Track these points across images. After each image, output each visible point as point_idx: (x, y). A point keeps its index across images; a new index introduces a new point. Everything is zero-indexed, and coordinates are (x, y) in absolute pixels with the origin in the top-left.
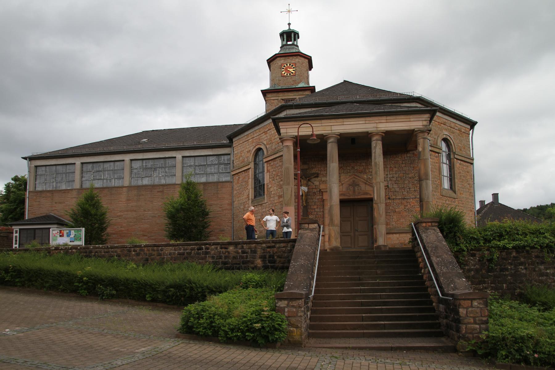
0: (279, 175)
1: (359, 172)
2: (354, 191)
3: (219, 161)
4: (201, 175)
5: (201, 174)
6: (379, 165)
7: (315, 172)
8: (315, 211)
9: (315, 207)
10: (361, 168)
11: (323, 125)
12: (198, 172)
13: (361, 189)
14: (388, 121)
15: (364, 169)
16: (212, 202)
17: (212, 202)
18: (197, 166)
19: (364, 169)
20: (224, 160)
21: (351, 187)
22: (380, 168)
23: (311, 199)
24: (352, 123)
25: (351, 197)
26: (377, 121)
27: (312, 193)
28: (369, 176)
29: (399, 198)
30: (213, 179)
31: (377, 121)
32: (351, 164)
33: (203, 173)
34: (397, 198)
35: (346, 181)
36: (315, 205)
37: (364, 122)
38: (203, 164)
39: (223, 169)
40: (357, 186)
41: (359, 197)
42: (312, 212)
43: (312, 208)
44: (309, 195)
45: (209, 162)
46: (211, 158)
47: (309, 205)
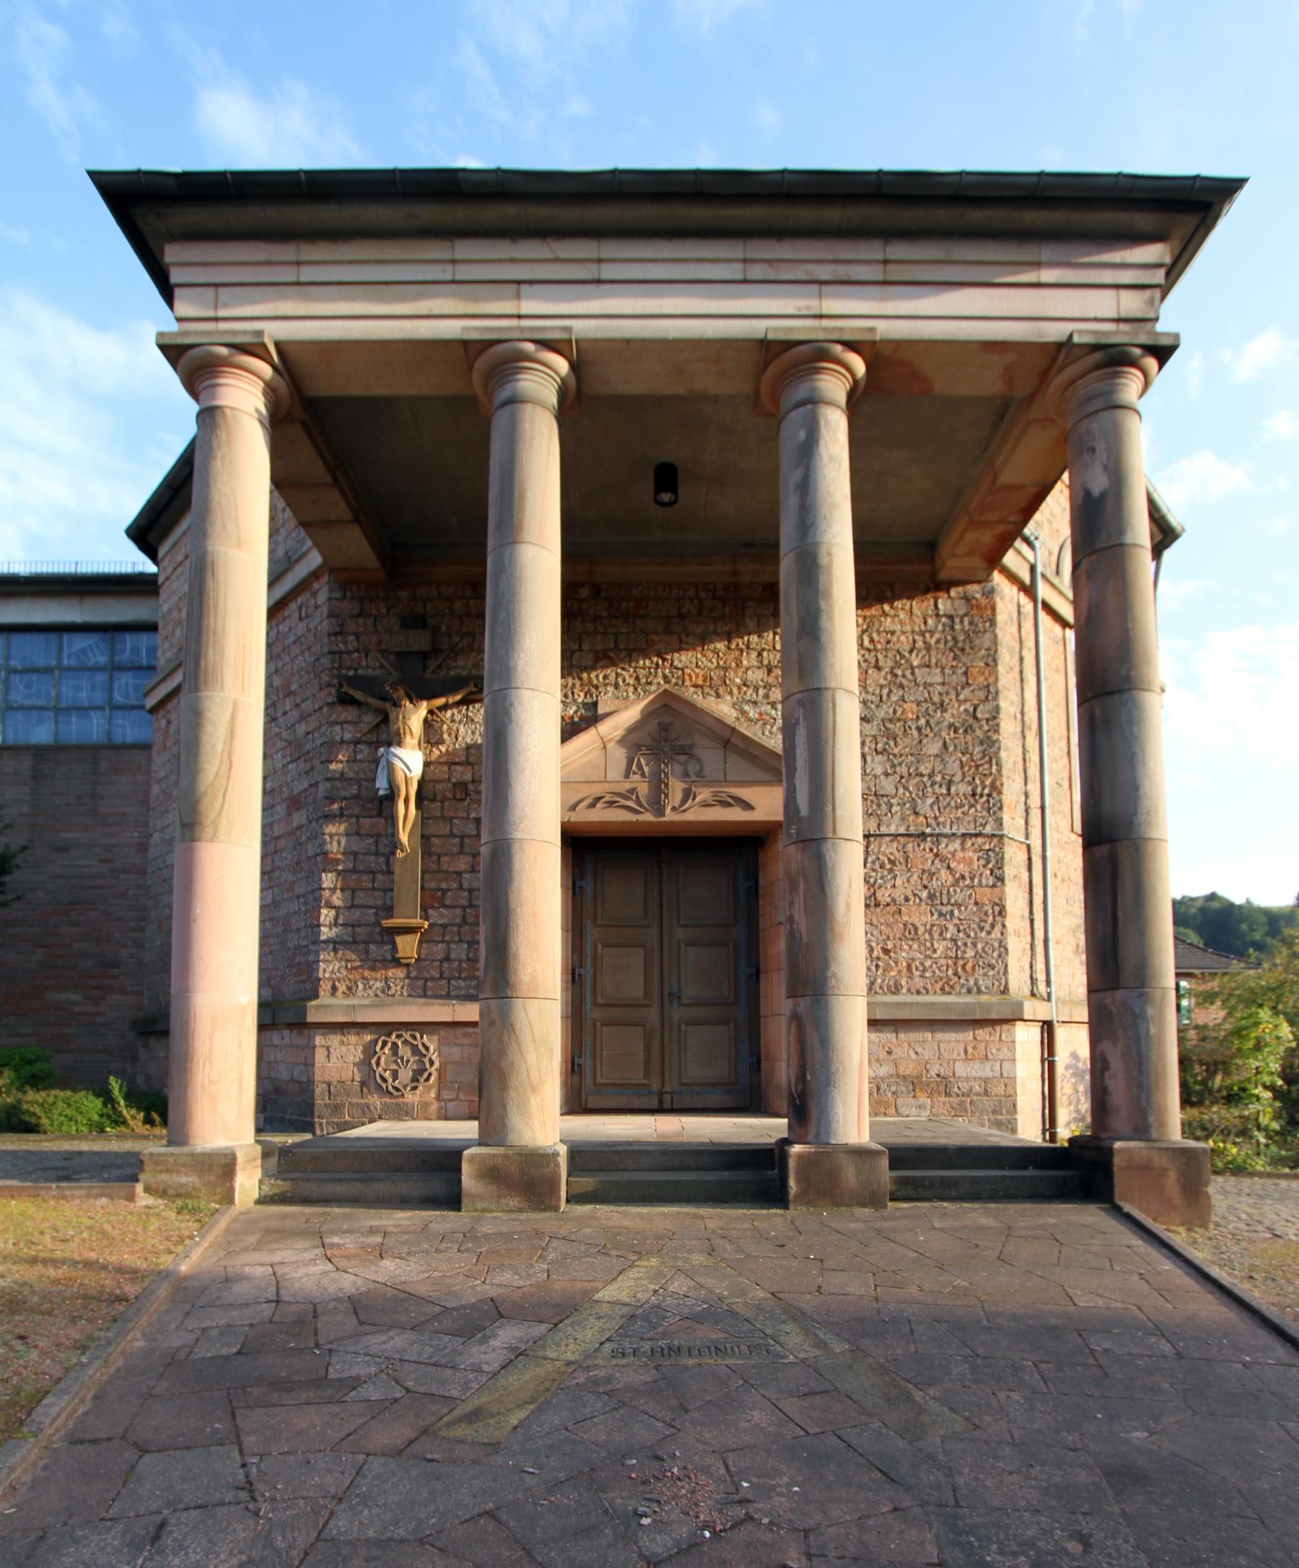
0: (293, 687)
3: (112, 655)
4: (35, 713)
5: (32, 708)
7: (465, 673)
8: (461, 888)
11: (464, 272)
12: (18, 698)
14: (895, 273)
16: (70, 835)
17: (70, 835)
18: (15, 671)
20: (135, 651)
23: (444, 818)
24: (665, 255)
26: (825, 272)
27: (450, 785)
29: (893, 829)
30: (92, 729)
31: (825, 272)
32: (656, 638)
33: (40, 702)
34: (884, 830)
36: (461, 852)
37: (735, 271)
38: (41, 662)
39: (131, 690)
40: (683, 758)
42: (444, 892)
43: (445, 867)
45: (69, 657)
46: (79, 642)
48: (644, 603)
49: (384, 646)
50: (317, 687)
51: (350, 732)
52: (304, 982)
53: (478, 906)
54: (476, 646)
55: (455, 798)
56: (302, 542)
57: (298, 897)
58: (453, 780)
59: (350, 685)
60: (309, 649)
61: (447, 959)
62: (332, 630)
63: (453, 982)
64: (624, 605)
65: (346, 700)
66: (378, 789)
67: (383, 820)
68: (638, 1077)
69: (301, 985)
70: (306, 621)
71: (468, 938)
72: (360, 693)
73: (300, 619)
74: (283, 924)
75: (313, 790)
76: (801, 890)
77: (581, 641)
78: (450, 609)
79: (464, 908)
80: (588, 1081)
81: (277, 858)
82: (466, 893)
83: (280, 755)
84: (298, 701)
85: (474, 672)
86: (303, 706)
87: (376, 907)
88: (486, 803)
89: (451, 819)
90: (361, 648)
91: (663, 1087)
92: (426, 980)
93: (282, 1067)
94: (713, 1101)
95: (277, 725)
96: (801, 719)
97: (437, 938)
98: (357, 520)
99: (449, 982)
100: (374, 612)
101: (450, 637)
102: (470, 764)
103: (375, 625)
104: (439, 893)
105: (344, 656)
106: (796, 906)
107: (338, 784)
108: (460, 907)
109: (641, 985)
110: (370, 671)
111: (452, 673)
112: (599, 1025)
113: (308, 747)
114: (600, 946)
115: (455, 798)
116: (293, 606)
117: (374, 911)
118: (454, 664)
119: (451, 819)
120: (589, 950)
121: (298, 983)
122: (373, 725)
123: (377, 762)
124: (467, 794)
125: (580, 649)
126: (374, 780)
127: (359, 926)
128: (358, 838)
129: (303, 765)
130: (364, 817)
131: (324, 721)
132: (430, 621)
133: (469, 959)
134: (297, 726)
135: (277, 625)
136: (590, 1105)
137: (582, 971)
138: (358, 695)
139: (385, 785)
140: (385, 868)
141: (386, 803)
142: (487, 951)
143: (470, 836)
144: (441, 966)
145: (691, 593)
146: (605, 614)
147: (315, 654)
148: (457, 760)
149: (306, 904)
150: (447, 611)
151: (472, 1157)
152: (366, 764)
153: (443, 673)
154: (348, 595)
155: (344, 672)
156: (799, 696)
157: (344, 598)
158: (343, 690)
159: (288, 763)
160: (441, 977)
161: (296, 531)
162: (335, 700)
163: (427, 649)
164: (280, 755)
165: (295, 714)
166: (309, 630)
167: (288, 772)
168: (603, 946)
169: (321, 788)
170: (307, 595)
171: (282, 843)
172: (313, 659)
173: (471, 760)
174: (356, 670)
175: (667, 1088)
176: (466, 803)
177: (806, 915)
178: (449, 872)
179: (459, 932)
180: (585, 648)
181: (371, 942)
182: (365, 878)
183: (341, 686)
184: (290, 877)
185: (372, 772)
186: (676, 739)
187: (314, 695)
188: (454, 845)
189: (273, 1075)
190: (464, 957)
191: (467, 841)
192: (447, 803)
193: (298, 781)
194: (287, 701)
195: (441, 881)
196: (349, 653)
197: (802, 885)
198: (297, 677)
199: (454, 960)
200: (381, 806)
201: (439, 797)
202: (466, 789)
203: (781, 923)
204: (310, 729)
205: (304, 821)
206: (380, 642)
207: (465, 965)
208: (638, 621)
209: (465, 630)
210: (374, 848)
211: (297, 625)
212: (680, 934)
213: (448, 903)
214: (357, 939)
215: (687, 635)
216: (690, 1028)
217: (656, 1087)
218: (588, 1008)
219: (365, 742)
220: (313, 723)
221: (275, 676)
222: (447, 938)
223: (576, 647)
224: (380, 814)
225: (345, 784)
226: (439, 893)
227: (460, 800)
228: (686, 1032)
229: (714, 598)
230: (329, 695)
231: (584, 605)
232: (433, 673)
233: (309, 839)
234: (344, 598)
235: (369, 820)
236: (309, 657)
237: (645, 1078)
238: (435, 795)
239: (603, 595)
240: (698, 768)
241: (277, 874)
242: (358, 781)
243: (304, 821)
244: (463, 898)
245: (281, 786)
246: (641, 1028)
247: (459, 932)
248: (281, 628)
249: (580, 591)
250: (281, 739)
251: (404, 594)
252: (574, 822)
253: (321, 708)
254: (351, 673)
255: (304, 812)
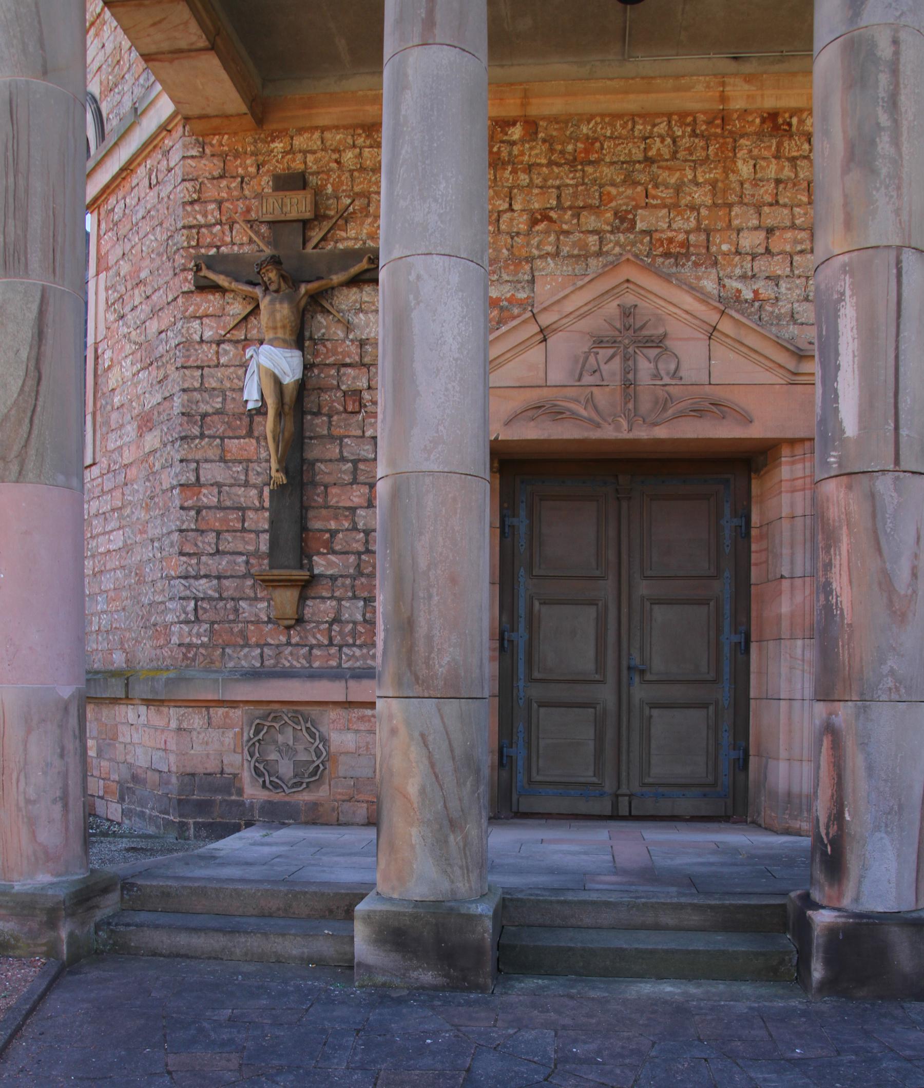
0: (143, 275)
1: (667, 255)
2: (629, 386)
6: (895, 72)
8: (355, 528)
9: (356, 500)
10: (685, 223)
13: (675, 374)
15: (698, 229)
19: (698, 229)
21: (604, 353)
22: (904, 99)
23: (331, 437)
25: (608, 433)
27: (339, 394)
28: (739, 285)
35: (569, 307)
36: (355, 481)
40: (653, 352)
41: (661, 433)
42: (333, 533)
43: (333, 501)
44: (318, 414)
47: (315, 484)
48: (597, 145)
49: (253, 215)
50: (171, 273)
51: (211, 328)
52: (161, 647)
53: (374, 553)
54: (372, 209)
55: (345, 411)
56: (149, 88)
57: (152, 541)
58: (344, 387)
59: (209, 268)
60: (161, 224)
61: (336, 620)
62: (188, 198)
63: (345, 650)
64: (570, 148)
65: (204, 287)
66: (247, 401)
67: (254, 441)
68: (587, 775)
69: (158, 651)
70: (156, 189)
71: (366, 594)
72: (222, 277)
73: (150, 187)
74: (137, 574)
75: (167, 404)
76: (844, 547)
77: (511, 199)
78: (338, 162)
79: (359, 554)
80: (521, 778)
81: (127, 491)
82: (362, 535)
83: (129, 361)
84: (149, 291)
85: (370, 243)
86: (154, 298)
87: (248, 554)
88: (383, 421)
89: (341, 439)
90: (224, 219)
91: (619, 788)
92: (312, 647)
93: (139, 751)
94: (685, 806)
95: (125, 324)
96: (848, 293)
97: (325, 594)
98: (213, 47)
99: (340, 650)
100: (240, 171)
101: (338, 198)
102: (364, 365)
103: (242, 188)
104: (327, 536)
105: (203, 230)
106: (835, 570)
107: (197, 396)
108: (353, 553)
109: (591, 653)
110: (236, 248)
111: (341, 246)
112: (535, 705)
113: (161, 349)
114: (536, 604)
115: (345, 411)
116: (142, 172)
117: (244, 558)
118: (343, 234)
119: (341, 439)
120: (522, 611)
121: (155, 648)
122: (241, 317)
123: (245, 366)
124: (362, 406)
125: (511, 209)
126: (242, 390)
127: (226, 578)
128: (222, 465)
129: (154, 373)
130: (230, 438)
131: (179, 316)
132: (313, 180)
133: (365, 621)
134: (147, 323)
135: (124, 198)
136: (523, 809)
137: (514, 636)
138: (222, 280)
139: (256, 396)
140: (257, 504)
141: (258, 419)
142: (386, 630)
143: (365, 460)
144: (330, 630)
145: (662, 128)
146: (544, 161)
147: (168, 230)
148: (348, 360)
149: (161, 549)
150: (334, 165)
151: (368, 918)
152: (232, 369)
153: (330, 246)
154: (208, 151)
155: (203, 251)
156: (846, 258)
157: (203, 155)
158: (202, 274)
159: (139, 372)
160: (331, 644)
161: (144, 76)
162: (193, 288)
163: (308, 215)
164: (129, 361)
165: (146, 308)
166: (160, 200)
167: (139, 382)
168: (540, 604)
169: (177, 401)
170: (158, 155)
171: (133, 472)
172: (165, 237)
173: (367, 360)
174: (218, 247)
175: (624, 790)
176: (360, 417)
177: (850, 582)
178: (338, 508)
179: (353, 587)
180: (517, 207)
181: (241, 599)
182: (233, 516)
183: (198, 268)
184: (143, 515)
185: (239, 379)
186: (642, 328)
187: (167, 283)
188: (344, 472)
189: (130, 759)
190: (359, 618)
191: (361, 466)
192: (335, 418)
193: (150, 393)
194: (136, 291)
195: (328, 520)
196: (209, 226)
197: (845, 539)
198: (147, 262)
199: (348, 622)
200: (251, 422)
201: (325, 410)
202: (361, 398)
203: (782, 577)
204: (163, 328)
205: (157, 445)
206: (248, 210)
207: (360, 629)
208: (589, 169)
209: (357, 189)
210: (243, 478)
211: (147, 194)
212: (644, 589)
213: (338, 548)
214: (225, 595)
215: (656, 186)
216: (655, 712)
217: (609, 786)
218: (521, 684)
219: (230, 341)
220: (166, 318)
221: (121, 262)
222: (337, 594)
223: (506, 206)
224: (250, 434)
225: (206, 395)
226: (327, 536)
227: (352, 413)
228: (651, 717)
229: (694, 134)
230: (187, 282)
231: (516, 150)
232: (314, 248)
233: (163, 467)
234: (203, 155)
235: (236, 441)
236: (160, 235)
237: (595, 776)
238: (320, 407)
239: (541, 135)
240: (673, 367)
241: (127, 511)
242: (223, 392)
243: (157, 445)
244: (357, 541)
245: (131, 401)
246: (591, 710)
247: (353, 587)
248: (128, 200)
249: (511, 131)
250: (130, 341)
251: (278, 146)
252: (502, 441)
253: (175, 299)
254: (213, 251)
255: (156, 433)
